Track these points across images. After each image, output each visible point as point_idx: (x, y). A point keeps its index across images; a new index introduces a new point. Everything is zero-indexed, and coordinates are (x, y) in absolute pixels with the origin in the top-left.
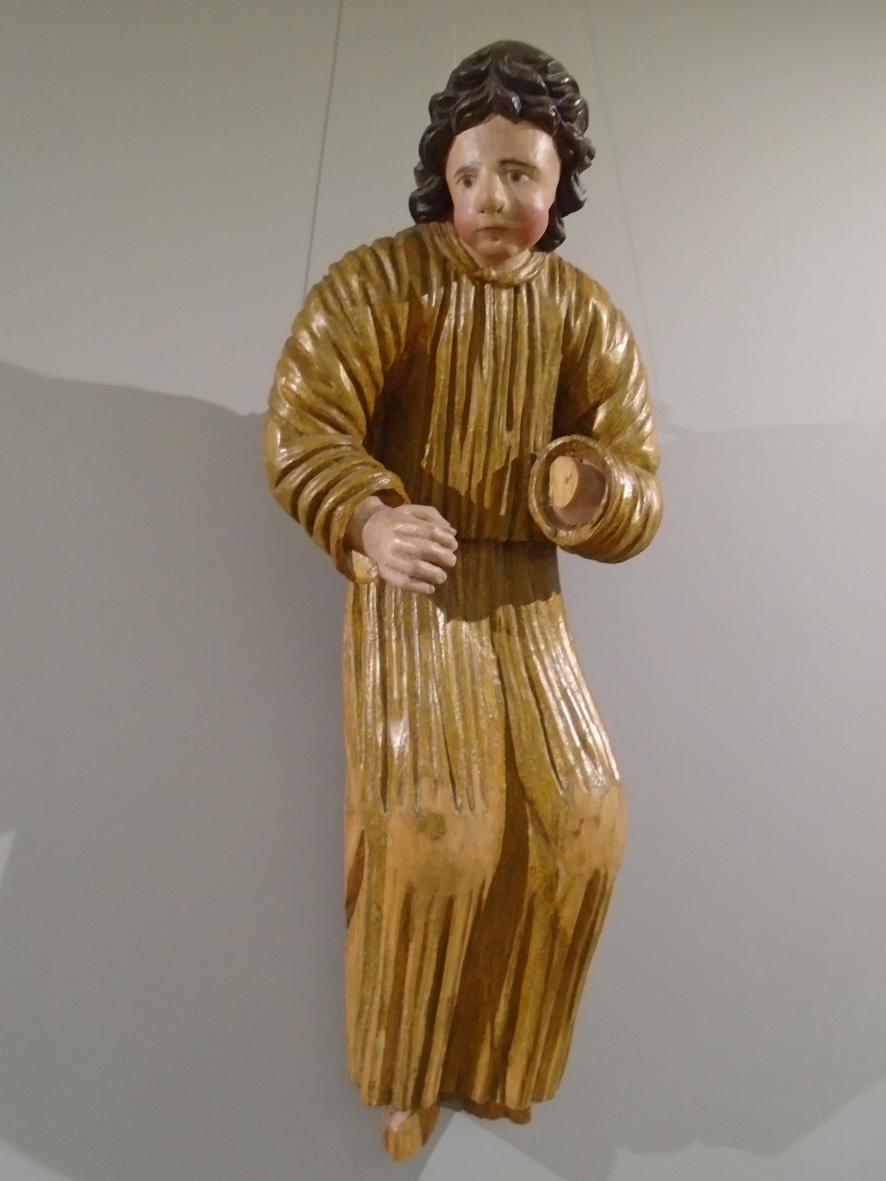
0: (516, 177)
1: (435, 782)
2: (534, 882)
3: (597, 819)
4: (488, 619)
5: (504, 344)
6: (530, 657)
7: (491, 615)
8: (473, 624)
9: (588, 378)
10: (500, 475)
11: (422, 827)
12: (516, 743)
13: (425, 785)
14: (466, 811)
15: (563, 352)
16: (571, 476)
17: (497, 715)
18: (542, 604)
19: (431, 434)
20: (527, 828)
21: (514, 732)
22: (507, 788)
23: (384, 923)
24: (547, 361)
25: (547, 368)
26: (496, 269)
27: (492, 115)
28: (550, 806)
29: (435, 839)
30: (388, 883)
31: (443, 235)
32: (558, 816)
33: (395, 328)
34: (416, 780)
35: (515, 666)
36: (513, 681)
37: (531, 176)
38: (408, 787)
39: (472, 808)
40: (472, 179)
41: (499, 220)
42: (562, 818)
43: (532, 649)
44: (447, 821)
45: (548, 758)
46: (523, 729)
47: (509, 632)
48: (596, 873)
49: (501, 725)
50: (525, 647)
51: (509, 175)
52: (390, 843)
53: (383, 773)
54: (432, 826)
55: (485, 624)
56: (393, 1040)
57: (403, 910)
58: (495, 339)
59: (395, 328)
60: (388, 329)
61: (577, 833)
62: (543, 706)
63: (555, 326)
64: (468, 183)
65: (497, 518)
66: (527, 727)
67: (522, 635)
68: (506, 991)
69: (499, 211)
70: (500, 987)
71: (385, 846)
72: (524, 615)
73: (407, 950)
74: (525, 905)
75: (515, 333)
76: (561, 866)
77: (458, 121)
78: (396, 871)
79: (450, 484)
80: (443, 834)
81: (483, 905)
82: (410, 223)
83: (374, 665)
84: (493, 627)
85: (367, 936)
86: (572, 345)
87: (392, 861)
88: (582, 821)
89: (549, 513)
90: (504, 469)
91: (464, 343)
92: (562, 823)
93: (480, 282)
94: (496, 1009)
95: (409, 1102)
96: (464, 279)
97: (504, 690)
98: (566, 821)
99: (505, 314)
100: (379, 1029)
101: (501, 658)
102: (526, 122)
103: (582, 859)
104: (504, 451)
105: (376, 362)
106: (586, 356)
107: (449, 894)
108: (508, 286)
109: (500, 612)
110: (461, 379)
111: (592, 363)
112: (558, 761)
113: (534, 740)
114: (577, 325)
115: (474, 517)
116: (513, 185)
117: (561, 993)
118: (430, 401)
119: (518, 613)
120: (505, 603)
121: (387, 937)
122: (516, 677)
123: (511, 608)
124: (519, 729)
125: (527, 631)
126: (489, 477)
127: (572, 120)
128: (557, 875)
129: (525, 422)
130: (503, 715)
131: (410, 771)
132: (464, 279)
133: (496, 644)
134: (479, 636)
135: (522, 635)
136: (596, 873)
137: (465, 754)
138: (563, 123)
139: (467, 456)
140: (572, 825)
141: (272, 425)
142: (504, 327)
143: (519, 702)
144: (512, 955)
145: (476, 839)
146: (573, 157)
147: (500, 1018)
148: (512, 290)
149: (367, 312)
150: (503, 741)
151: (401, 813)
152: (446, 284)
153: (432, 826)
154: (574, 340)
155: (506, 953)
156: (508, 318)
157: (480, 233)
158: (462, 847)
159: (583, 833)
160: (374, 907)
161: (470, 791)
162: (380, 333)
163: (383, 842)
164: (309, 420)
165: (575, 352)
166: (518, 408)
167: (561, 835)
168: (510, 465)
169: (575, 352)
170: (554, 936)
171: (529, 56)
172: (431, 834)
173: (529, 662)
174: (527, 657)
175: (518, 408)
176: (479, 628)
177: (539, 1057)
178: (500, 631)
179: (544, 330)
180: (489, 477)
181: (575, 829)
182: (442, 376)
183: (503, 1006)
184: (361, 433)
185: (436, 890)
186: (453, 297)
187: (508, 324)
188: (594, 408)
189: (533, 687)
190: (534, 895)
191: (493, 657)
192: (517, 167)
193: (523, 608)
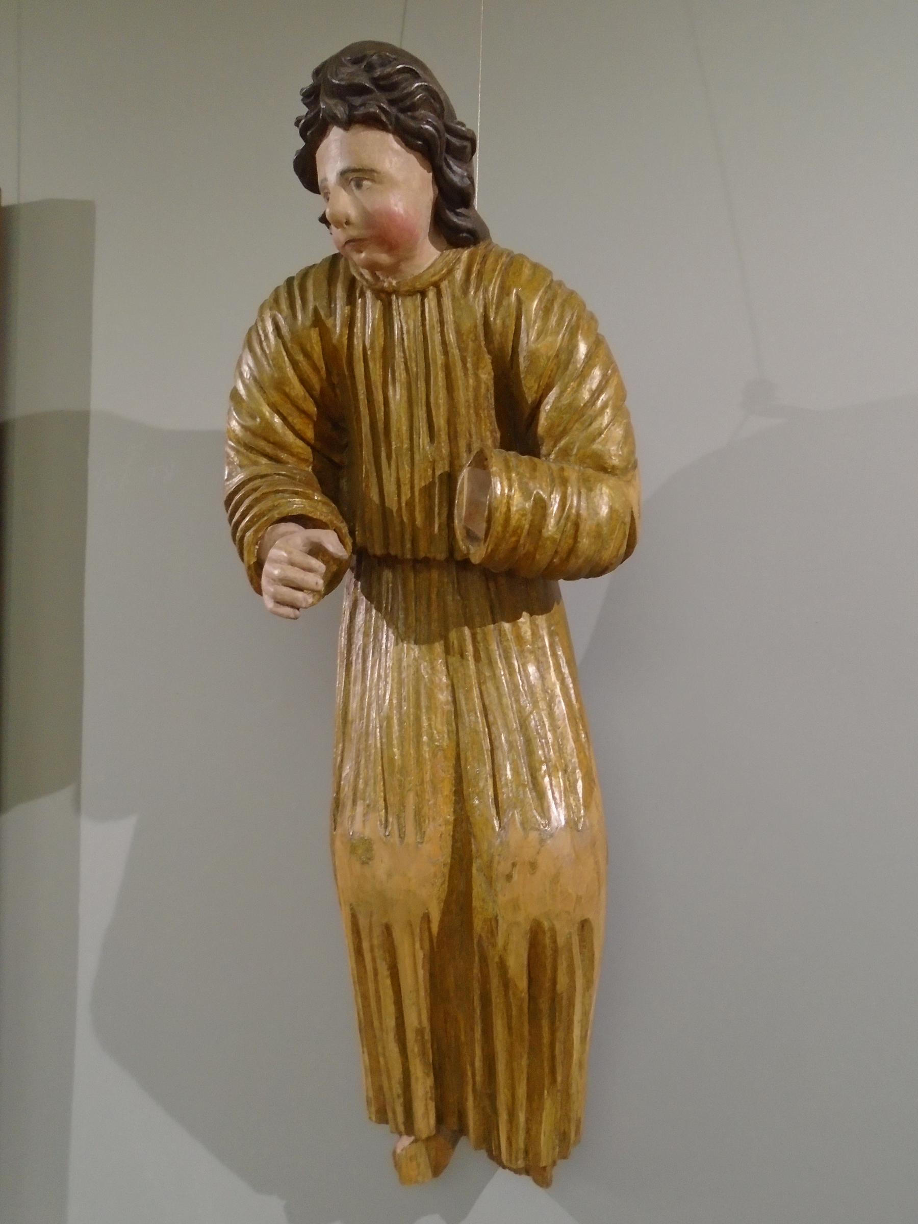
0: (359, 186)
3: (533, 866)
4: (442, 642)
7: (445, 638)
8: (424, 647)
9: (522, 376)
10: (428, 491)
15: (489, 352)
18: (507, 626)
22: (455, 820)
24: (469, 365)
25: (470, 372)
26: (395, 278)
29: (363, 863)
33: (307, 355)
34: (354, 802)
35: (469, 692)
37: (373, 181)
39: (402, 837)
41: (353, 233)
43: (487, 674)
44: (375, 847)
45: (491, 792)
47: (462, 655)
49: (451, 754)
55: (439, 647)
57: (353, 931)
59: (307, 355)
60: (300, 358)
61: (509, 877)
65: (431, 538)
67: (477, 659)
69: (348, 223)
79: (387, 504)
81: (435, 941)
84: (447, 651)
86: (496, 342)
88: (514, 865)
90: (432, 484)
91: (374, 359)
92: (495, 865)
93: (385, 297)
95: (402, 1128)
101: (455, 681)
102: (357, 126)
103: (515, 906)
105: (297, 390)
108: (411, 293)
109: (453, 635)
110: (380, 398)
114: (497, 322)
115: (408, 537)
117: (534, 1049)
120: (459, 625)
123: (467, 631)
125: (482, 655)
126: (417, 493)
127: (413, 107)
129: (452, 433)
130: (454, 744)
132: (369, 294)
133: (451, 668)
134: (430, 659)
137: (400, 781)
138: (402, 116)
139: (394, 474)
146: (443, 148)
150: (452, 771)
152: (351, 301)
158: (389, 875)
159: (516, 877)
161: (402, 819)
162: (295, 364)
166: (441, 421)
167: (494, 877)
168: (437, 481)
169: (502, 349)
171: (387, 53)
175: (441, 421)
176: (431, 651)
177: (522, 1117)
179: (458, 333)
180: (417, 493)
181: (507, 872)
184: (305, 461)
185: (371, 916)
186: (359, 314)
193: (478, 630)
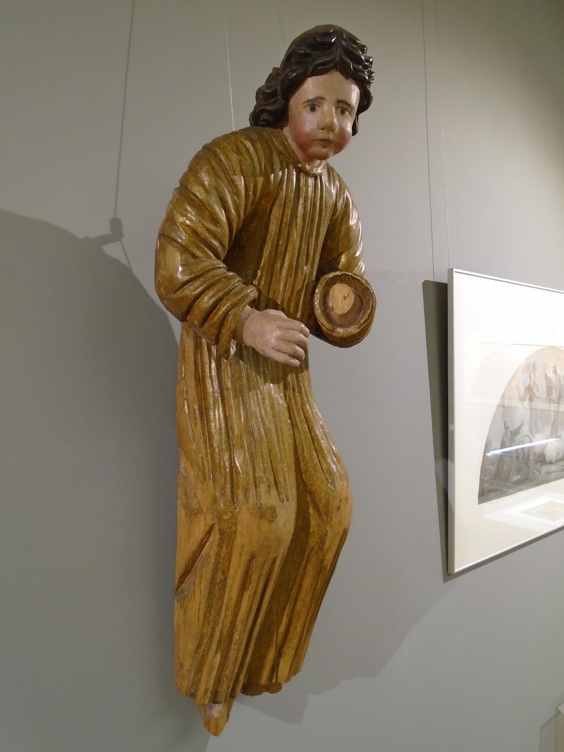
0: (343, 112)
1: (268, 486)
2: (313, 541)
5: (309, 211)
6: (305, 405)
11: (262, 516)
12: (301, 458)
13: (263, 488)
14: (286, 502)
16: (348, 296)
17: (290, 441)
19: (262, 264)
20: (309, 508)
21: (300, 451)
23: (229, 582)
26: (309, 165)
27: (334, 70)
28: (323, 494)
29: (271, 522)
30: (235, 556)
31: (277, 137)
32: (329, 499)
36: (298, 420)
38: (252, 492)
40: (317, 107)
41: (331, 136)
42: (331, 499)
44: (277, 510)
46: (305, 449)
47: (294, 390)
48: (346, 529)
50: (302, 399)
51: (339, 109)
52: (239, 529)
53: (231, 484)
54: (267, 514)
56: (225, 658)
58: (305, 208)
61: (339, 508)
62: (313, 434)
63: (331, 202)
64: (313, 109)
66: (307, 448)
68: (287, 611)
70: (284, 609)
71: (235, 532)
72: (301, 379)
73: (242, 596)
74: (306, 556)
75: (315, 204)
76: (328, 528)
77: (314, 69)
78: (243, 547)
80: (275, 518)
82: (248, 125)
83: (219, 413)
84: (286, 388)
85: (211, 593)
87: (239, 541)
88: (341, 500)
89: (328, 317)
92: (331, 503)
93: (300, 171)
94: (280, 623)
96: (291, 167)
97: (292, 425)
98: (333, 502)
99: (310, 193)
100: (216, 652)
103: (340, 523)
104: (303, 277)
106: (341, 224)
107: (274, 556)
109: (289, 378)
111: (343, 228)
112: (325, 466)
113: (311, 455)
116: (340, 116)
118: (264, 242)
119: (297, 378)
121: (231, 591)
122: (299, 418)
124: (303, 449)
128: (326, 534)
131: (252, 481)
132: (291, 167)
133: (288, 398)
135: (300, 392)
136: (346, 529)
140: (336, 504)
141: (171, 249)
142: (309, 201)
143: (302, 432)
144: (294, 588)
145: (286, 521)
147: (282, 628)
148: (313, 179)
149: (241, 180)
151: (248, 509)
153: (267, 514)
154: (337, 214)
155: (290, 587)
156: (312, 195)
157: (316, 142)
158: (284, 525)
159: (341, 507)
160: (220, 573)
163: (234, 529)
164: (203, 249)
165: (336, 220)
167: (330, 510)
169: (336, 220)
170: (320, 572)
172: (269, 519)
173: (304, 408)
174: (303, 405)
176: (279, 387)
178: (289, 390)
182: (273, 228)
183: (285, 621)
187: (311, 199)
188: (340, 255)
189: (307, 423)
190: (312, 548)
191: (286, 405)
192: (345, 106)
